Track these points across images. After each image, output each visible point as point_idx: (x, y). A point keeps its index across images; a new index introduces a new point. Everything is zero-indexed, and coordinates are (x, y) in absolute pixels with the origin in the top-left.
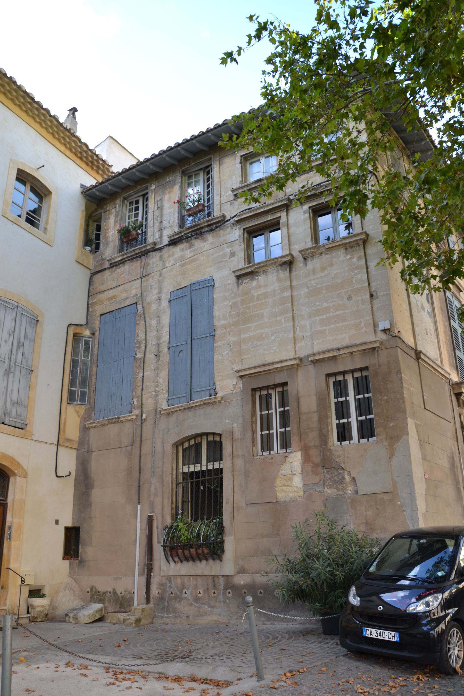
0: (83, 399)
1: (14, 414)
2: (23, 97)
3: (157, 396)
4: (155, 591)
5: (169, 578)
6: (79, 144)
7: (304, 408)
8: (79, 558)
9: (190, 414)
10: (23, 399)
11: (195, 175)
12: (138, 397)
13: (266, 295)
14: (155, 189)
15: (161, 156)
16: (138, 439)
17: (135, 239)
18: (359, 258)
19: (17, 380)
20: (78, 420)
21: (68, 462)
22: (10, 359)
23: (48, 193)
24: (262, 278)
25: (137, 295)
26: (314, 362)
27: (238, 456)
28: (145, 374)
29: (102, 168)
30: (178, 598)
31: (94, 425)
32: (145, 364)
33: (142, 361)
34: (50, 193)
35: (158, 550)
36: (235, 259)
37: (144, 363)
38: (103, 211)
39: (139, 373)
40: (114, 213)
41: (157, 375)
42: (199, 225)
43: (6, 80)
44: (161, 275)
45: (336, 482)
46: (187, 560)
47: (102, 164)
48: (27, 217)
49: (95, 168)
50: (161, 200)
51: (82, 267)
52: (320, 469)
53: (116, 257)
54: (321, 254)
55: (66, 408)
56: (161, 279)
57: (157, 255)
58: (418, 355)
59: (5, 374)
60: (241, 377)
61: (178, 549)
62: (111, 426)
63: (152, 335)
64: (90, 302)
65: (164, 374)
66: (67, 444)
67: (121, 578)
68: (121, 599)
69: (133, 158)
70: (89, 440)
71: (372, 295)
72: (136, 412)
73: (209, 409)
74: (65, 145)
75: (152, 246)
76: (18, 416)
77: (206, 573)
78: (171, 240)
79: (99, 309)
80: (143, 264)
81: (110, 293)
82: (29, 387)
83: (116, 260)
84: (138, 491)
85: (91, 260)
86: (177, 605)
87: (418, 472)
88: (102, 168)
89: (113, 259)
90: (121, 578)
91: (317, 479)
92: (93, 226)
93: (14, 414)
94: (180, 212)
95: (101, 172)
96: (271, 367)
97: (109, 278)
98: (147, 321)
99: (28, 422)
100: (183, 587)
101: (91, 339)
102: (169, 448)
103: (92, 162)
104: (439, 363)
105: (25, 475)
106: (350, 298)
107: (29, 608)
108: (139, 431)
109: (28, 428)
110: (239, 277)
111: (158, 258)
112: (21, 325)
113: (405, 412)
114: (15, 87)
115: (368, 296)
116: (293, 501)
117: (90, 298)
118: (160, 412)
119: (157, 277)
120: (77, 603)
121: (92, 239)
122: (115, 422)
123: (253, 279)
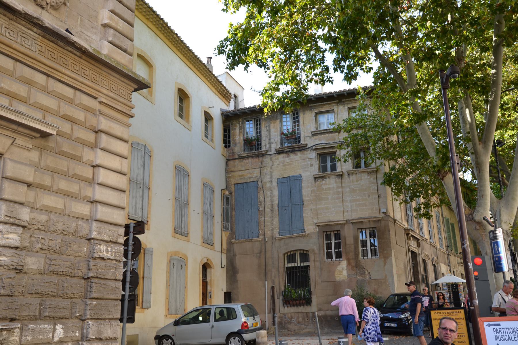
4: (276, 319)
5: (284, 314)
7: (348, 242)
9: (292, 240)
13: (329, 189)
16: (264, 250)
18: (374, 179)
24: (327, 180)
26: (352, 223)
27: (317, 261)
30: (290, 323)
35: (279, 302)
36: (313, 168)
42: (292, 144)
44: (271, 168)
45: (362, 274)
46: (294, 306)
50: (269, 126)
52: (355, 268)
54: (356, 173)
56: (271, 170)
57: (269, 157)
58: (395, 221)
60: (318, 226)
61: (288, 301)
62: (247, 243)
63: (268, 199)
65: (276, 221)
71: (379, 196)
72: (261, 237)
73: (301, 239)
77: (303, 311)
79: (233, 181)
81: (241, 173)
84: (265, 275)
86: (289, 326)
87: (395, 272)
91: (353, 272)
96: (333, 223)
97: (238, 165)
100: (292, 317)
102: (281, 255)
104: (401, 221)
106: (369, 196)
110: (315, 178)
113: (391, 247)
115: (377, 196)
116: (343, 281)
119: (269, 169)
121: (227, 141)
123: (323, 180)
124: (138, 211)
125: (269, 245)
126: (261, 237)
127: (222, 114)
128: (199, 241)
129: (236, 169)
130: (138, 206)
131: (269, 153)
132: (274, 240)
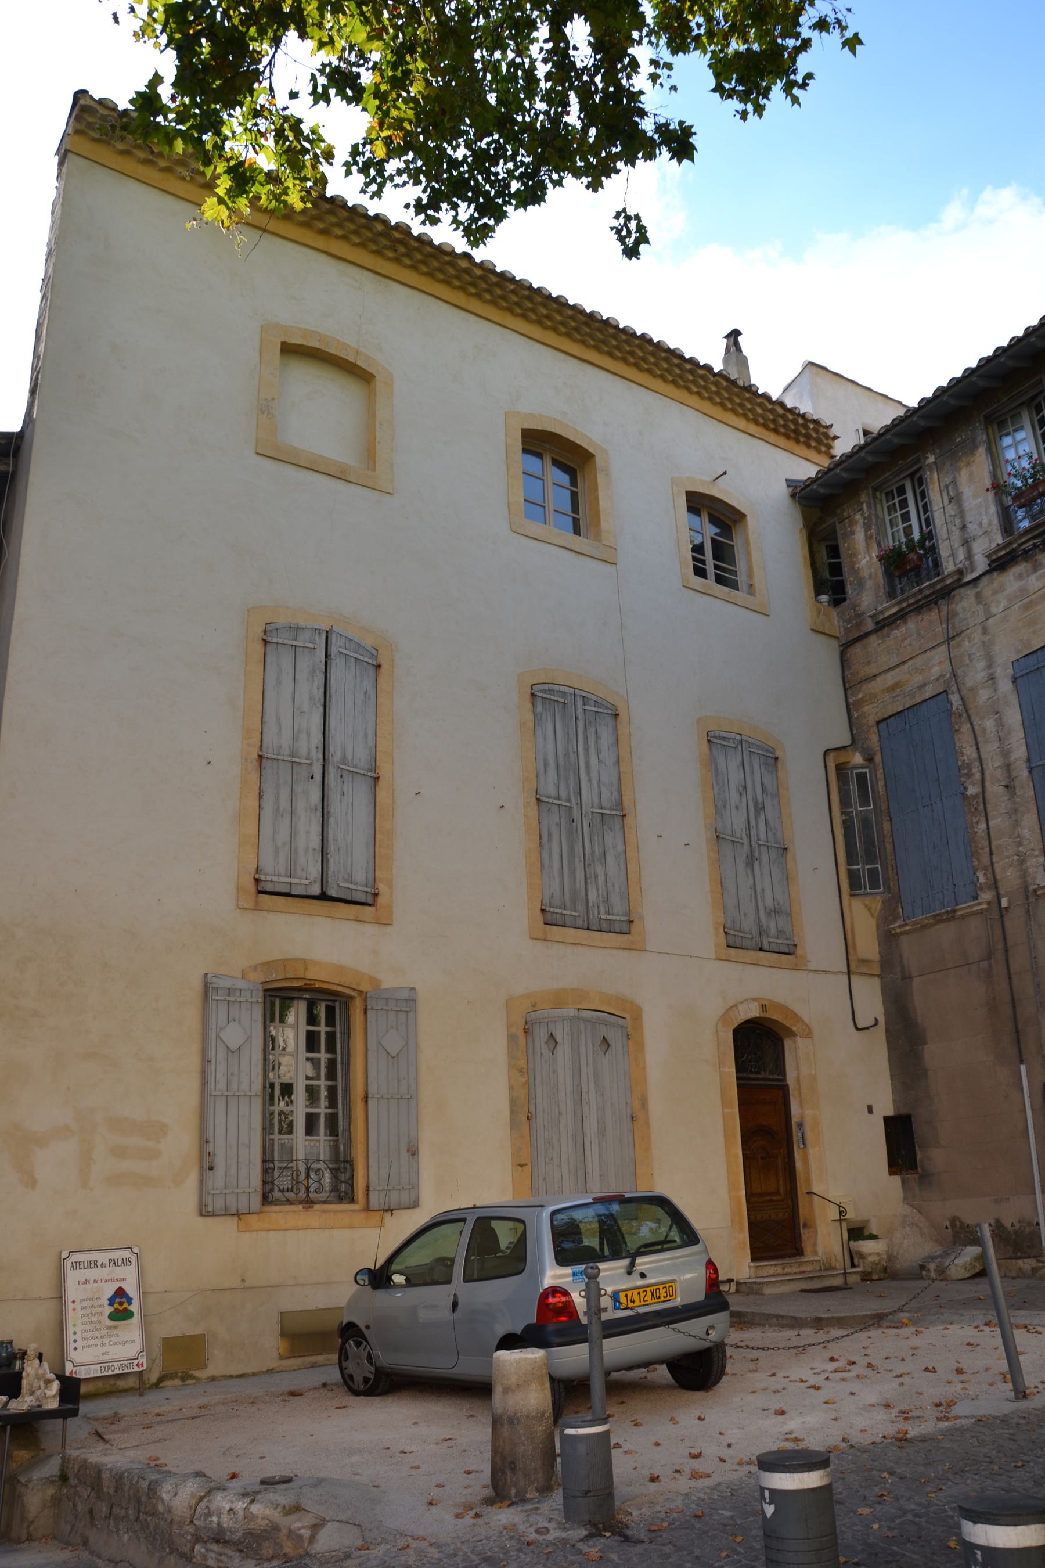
0: (874, 884)
1: (773, 931)
2: (666, 359)
3: (1022, 862)
6: (770, 407)
8: (919, 1170)
10: (781, 902)
11: (1012, 417)
12: (985, 868)
14: (935, 463)
15: (938, 400)
16: (1000, 946)
17: (917, 569)
19: (766, 870)
20: (873, 922)
21: (871, 1001)
22: (749, 837)
23: (738, 517)
25: (944, 676)
28: (991, 823)
29: (815, 435)
31: (907, 928)
32: (988, 806)
33: (981, 800)
34: (743, 516)
37: (984, 803)
38: (836, 519)
39: (977, 823)
40: (861, 521)
41: (1017, 823)
43: (637, 342)
44: (985, 631)
47: (814, 429)
48: (695, 566)
49: (802, 439)
50: (954, 482)
51: (823, 638)
53: (886, 609)
55: (850, 905)
56: (986, 638)
57: (970, 593)
59: (747, 864)
63: (990, 749)
64: (851, 700)
65: (1029, 821)
66: (864, 970)
67: (1008, 1199)
68: (1014, 1237)
69: (859, 389)
70: (901, 956)
72: (986, 896)
74: (745, 416)
75: (956, 577)
76: (781, 932)
78: (993, 561)
79: (872, 712)
80: (944, 613)
81: (890, 679)
82: (787, 878)
83: (887, 614)
85: (834, 621)
88: (815, 435)
89: (882, 612)
90: (1008, 1199)
92: (823, 555)
93: (773, 931)
94: (1000, 503)
95: (813, 444)
97: (879, 651)
98: (975, 723)
99: (796, 940)
101: (867, 770)
103: (795, 431)
105: (809, 1035)
107: (853, 1258)
108: (998, 932)
109: (799, 951)
111: (973, 599)
112: (752, 773)
114: (651, 348)
117: (849, 692)
118: (1035, 891)
119: (977, 635)
120: (929, 1248)
121: (830, 579)
122: (948, 920)
124: (302, 860)
125: (1015, 923)
126: (986, 896)
127: (793, 496)
128: (705, 937)
129: (873, 670)
130: (301, 842)
131: (969, 577)
132: (1032, 899)
